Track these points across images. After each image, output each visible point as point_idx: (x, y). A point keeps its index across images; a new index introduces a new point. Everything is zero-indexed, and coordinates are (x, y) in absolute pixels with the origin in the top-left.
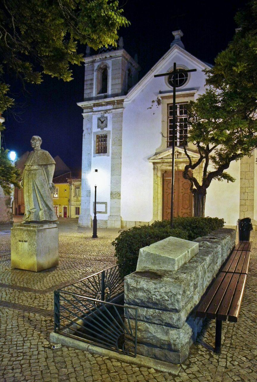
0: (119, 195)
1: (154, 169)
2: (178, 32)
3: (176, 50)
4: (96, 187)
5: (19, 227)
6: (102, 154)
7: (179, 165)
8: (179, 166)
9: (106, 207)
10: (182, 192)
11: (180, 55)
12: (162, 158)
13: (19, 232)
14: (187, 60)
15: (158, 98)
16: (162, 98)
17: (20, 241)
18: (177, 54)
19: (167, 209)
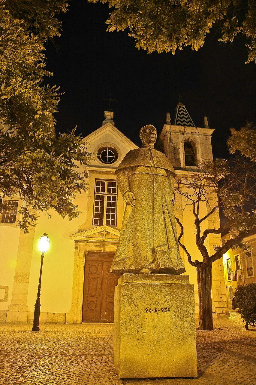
0: (27, 277)
1: (76, 248)
2: (111, 113)
3: (108, 128)
4: (43, 257)
5: (141, 281)
6: (8, 224)
7: (106, 246)
8: (106, 247)
9: (7, 293)
10: (107, 278)
11: (111, 134)
12: (86, 237)
13: (146, 291)
14: (118, 140)
15: (85, 171)
16: (90, 171)
17: (148, 311)
18: (108, 132)
19: (87, 297)
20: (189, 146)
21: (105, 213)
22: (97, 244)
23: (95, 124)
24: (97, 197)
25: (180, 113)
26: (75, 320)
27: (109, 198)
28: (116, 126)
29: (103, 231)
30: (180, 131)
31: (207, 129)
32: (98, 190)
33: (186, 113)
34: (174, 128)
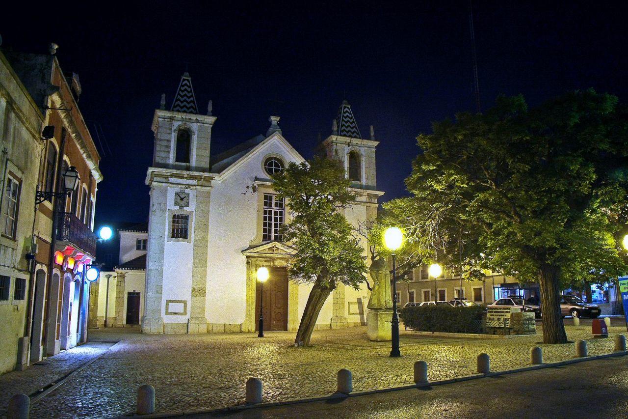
1: (248, 263)
6: (181, 239)
8: (275, 262)
9: (185, 307)
10: (275, 291)
12: (257, 252)
15: (253, 184)
20: (354, 157)
21: (273, 228)
22: (267, 259)
23: (264, 132)
24: (265, 212)
25: (183, 89)
26: (250, 329)
27: (276, 213)
28: (283, 135)
29: (273, 247)
30: (346, 142)
31: (373, 142)
32: (265, 204)
33: (189, 90)
34: (341, 139)
